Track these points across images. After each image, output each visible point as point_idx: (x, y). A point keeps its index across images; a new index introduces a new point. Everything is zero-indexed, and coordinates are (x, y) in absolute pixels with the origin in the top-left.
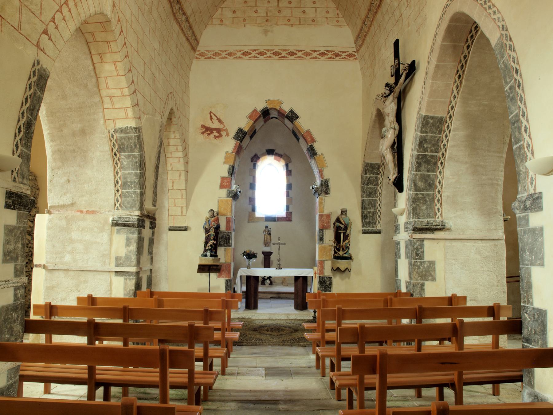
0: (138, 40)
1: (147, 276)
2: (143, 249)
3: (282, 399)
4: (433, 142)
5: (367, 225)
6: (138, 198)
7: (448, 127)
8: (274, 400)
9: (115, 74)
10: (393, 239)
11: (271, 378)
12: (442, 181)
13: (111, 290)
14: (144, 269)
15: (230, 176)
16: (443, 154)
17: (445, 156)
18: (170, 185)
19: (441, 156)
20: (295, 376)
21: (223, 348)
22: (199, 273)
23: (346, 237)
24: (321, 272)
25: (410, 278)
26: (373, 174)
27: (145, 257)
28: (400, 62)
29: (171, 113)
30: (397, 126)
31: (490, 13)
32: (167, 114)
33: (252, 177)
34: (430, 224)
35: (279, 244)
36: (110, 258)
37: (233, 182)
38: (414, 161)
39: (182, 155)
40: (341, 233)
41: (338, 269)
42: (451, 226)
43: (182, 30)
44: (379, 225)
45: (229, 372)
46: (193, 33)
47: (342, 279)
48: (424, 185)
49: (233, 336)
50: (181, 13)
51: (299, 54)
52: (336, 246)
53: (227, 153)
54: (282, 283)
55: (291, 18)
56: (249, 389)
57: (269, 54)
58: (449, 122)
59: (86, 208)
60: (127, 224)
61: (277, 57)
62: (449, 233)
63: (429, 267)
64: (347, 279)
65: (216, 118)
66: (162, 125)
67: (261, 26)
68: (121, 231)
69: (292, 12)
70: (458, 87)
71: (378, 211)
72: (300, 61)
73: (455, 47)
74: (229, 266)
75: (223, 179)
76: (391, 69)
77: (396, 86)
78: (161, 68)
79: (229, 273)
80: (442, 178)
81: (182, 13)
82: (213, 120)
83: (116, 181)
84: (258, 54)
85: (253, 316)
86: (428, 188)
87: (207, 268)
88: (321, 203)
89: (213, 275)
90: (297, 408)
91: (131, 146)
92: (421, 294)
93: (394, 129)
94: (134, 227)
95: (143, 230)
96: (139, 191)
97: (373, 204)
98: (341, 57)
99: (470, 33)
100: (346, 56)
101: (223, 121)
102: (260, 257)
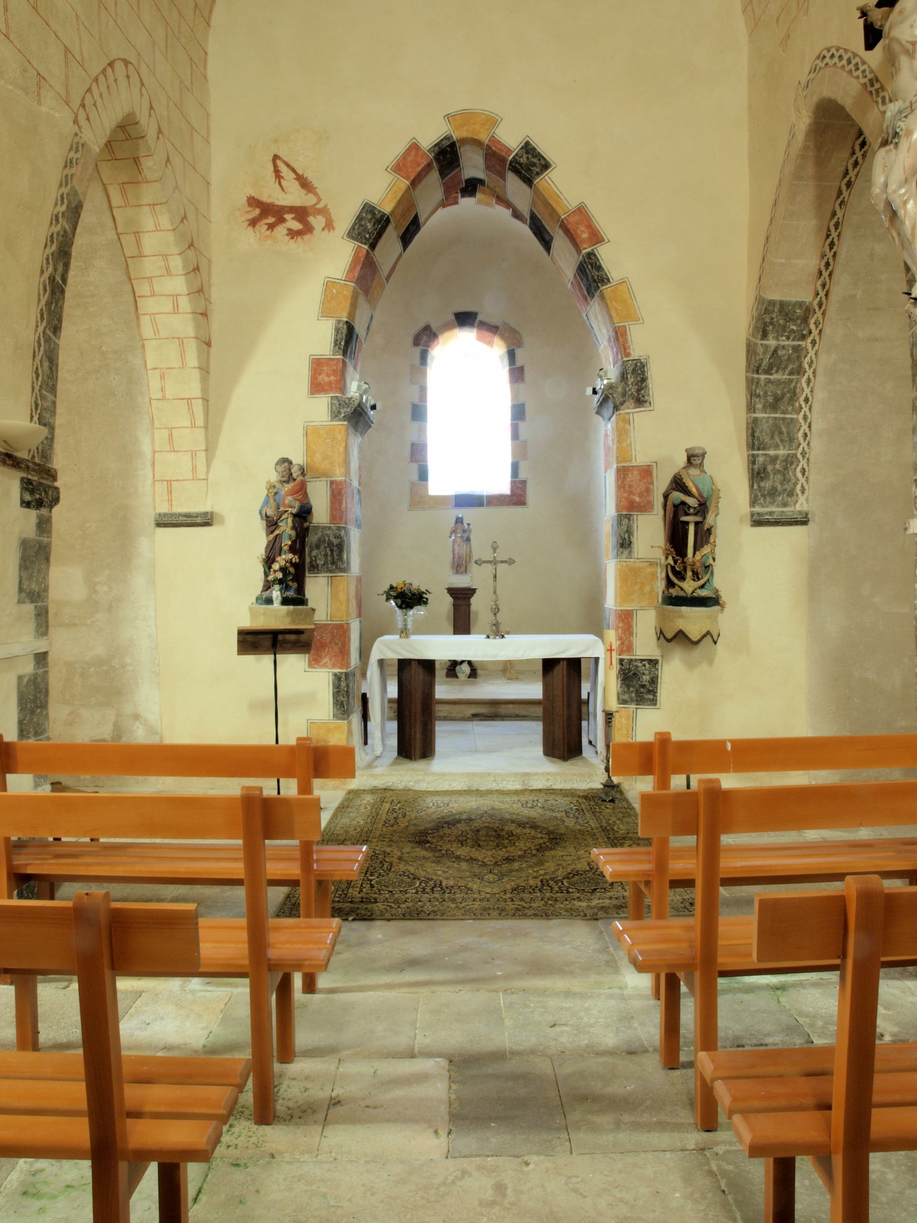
1: (20, 678)
5: (765, 500)
10: (910, 531)
15: (341, 352)
18: (154, 384)
23: (704, 535)
24: (626, 644)
26: (788, 338)
35: (494, 562)
39: (185, 287)
40: (687, 523)
41: (681, 637)
44: (802, 499)
47: (691, 666)
52: (672, 563)
53: (329, 284)
64: (705, 666)
65: (293, 176)
71: (800, 456)
74: (342, 631)
75: (317, 364)
79: (344, 652)
82: (283, 183)
87: (268, 641)
101: (315, 183)
102: (441, 604)
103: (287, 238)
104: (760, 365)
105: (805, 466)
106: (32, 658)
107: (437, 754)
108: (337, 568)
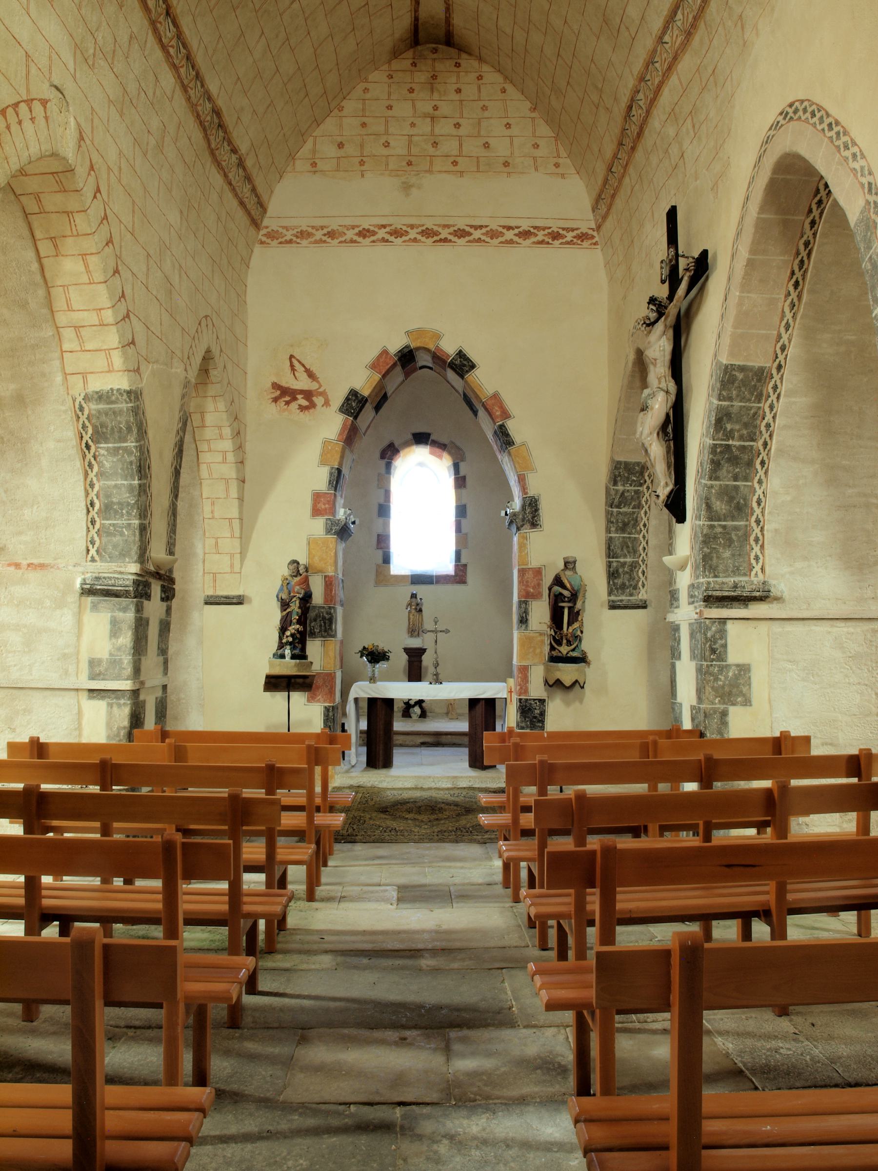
0: (133, 207)
1: (156, 698)
2: (147, 643)
3: (428, 948)
4: (745, 419)
5: (617, 592)
6: (135, 537)
7: (775, 388)
8: (410, 950)
9: (85, 279)
10: (667, 620)
11: (408, 906)
12: (763, 499)
13: (79, 728)
14: (148, 684)
15: (333, 489)
16: (765, 444)
17: (770, 449)
18: (207, 508)
19: (761, 448)
20: (457, 902)
21: (310, 845)
22: (268, 694)
23: (575, 616)
25: (700, 699)
26: (631, 485)
27: (152, 659)
28: (680, 252)
29: (208, 357)
30: (672, 387)
31: (847, 158)
32: (197, 360)
33: (382, 491)
34: (739, 589)
36: (78, 662)
37: (340, 501)
38: (706, 458)
40: (563, 607)
41: (558, 683)
42: (782, 592)
43: (230, 184)
44: (643, 591)
45: (324, 894)
46: (254, 190)
47: (568, 704)
48: (728, 507)
49: (331, 820)
50: (227, 148)
51: (477, 234)
52: (553, 634)
53: (326, 443)
54: (447, 714)
55: (459, 159)
56: (361, 928)
57: (413, 234)
58: (776, 377)
59: (26, 559)
60: (113, 590)
61: (431, 240)
62: (780, 605)
63: (737, 677)
64: (577, 704)
66: (187, 384)
67: (397, 176)
68: (101, 605)
69: (461, 145)
70: (794, 305)
71: (641, 563)
72: (476, 248)
73: (785, 224)
74: (331, 677)
75: (317, 497)
76: (662, 268)
77: (670, 303)
78: (183, 265)
79: (332, 692)
80: (763, 493)
81: (229, 148)
83: (89, 502)
84: (391, 234)
85: (381, 782)
86: (736, 514)
88: (522, 546)
89: (298, 698)
90: (456, 965)
91: (121, 428)
92: (720, 732)
93: (667, 392)
94: (128, 597)
95: (146, 602)
96: (137, 522)
97: (631, 547)
98: (564, 241)
99: (815, 196)
100: (575, 237)
101: (318, 375)
102: (400, 660)
103: (298, 411)
104: (613, 502)
105: (645, 569)
106: (161, 687)
107: (394, 766)
108: (328, 634)
